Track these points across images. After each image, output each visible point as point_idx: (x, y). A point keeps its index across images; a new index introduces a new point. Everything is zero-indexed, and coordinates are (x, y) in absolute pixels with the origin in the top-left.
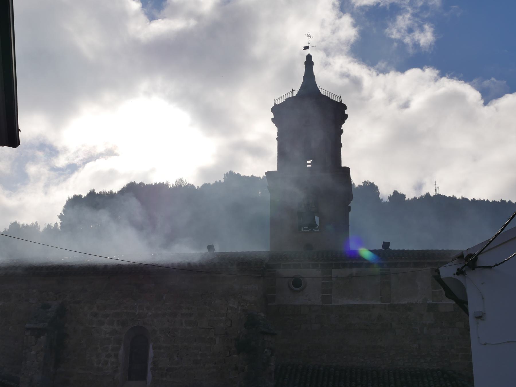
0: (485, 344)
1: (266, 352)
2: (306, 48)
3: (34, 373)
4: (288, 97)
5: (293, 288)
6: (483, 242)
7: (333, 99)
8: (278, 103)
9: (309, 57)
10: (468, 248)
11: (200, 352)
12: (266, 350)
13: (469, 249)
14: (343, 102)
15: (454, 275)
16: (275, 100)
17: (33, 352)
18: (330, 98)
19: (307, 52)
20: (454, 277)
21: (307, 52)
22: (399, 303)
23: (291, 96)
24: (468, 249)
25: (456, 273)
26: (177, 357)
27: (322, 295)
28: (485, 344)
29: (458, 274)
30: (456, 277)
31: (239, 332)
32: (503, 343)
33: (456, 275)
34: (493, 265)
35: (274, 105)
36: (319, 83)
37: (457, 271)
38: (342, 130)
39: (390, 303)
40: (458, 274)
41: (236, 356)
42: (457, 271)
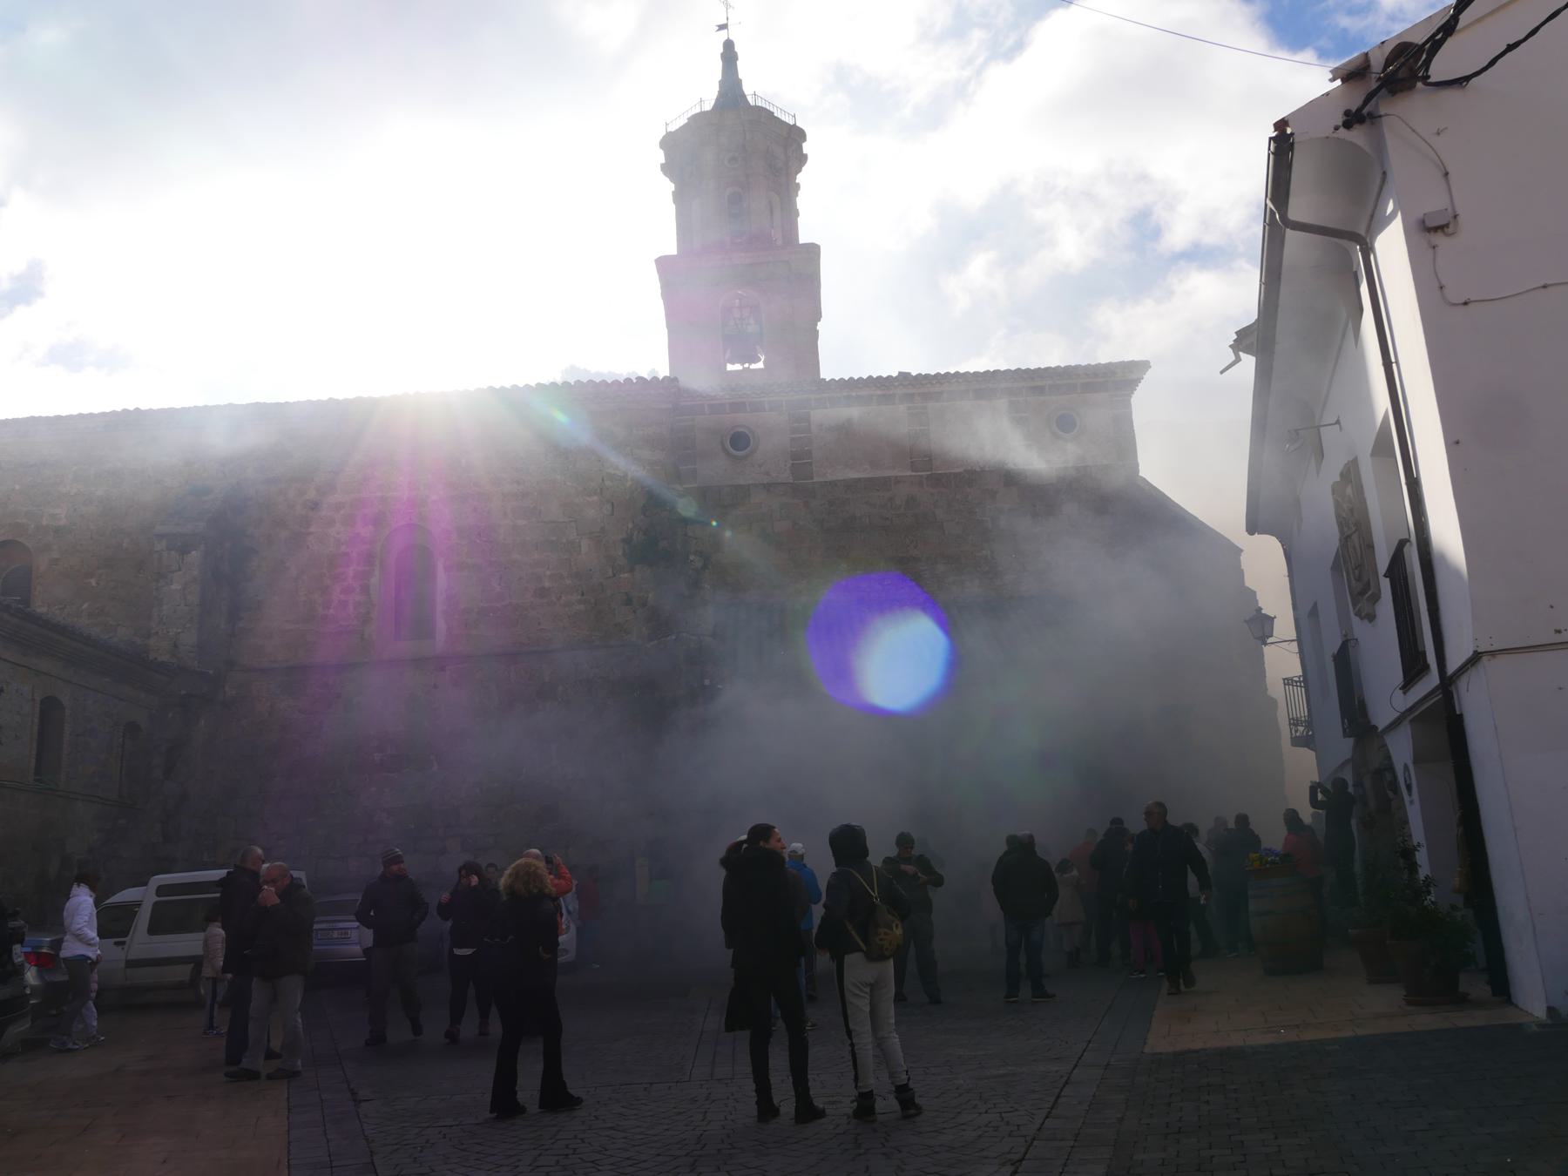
0: (1466, 303)
1: (692, 561)
2: (723, 27)
3: (179, 630)
4: (693, 113)
5: (735, 452)
6: (1430, 17)
7: (779, 116)
8: (672, 128)
9: (729, 46)
10: (1384, 40)
11: (548, 573)
12: (692, 557)
13: (1385, 44)
14: (797, 125)
15: (1336, 128)
16: (667, 124)
17: (174, 587)
18: (776, 115)
19: (723, 35)
20: (1335, 135)
21: (723, 35)
22: (947, 471)
23: (698, 110)
24: (1383, 43)
25: (1340, 124)
26: (499, 585)
27: (791, 462)
28: (1466, 303)
29: (1348, 125)
30: (1343, 132)
31: (630, 526)
32: (1534, 289)
33: (1342, 130)
34: (1522, 37)
35: (664, 133)
36: (748, 89)
37: (1345, 118)
38: (798, 184)
39: (929, 473)
40: (1348, 125)
41: (626, 575)
42: (1345, 118)
